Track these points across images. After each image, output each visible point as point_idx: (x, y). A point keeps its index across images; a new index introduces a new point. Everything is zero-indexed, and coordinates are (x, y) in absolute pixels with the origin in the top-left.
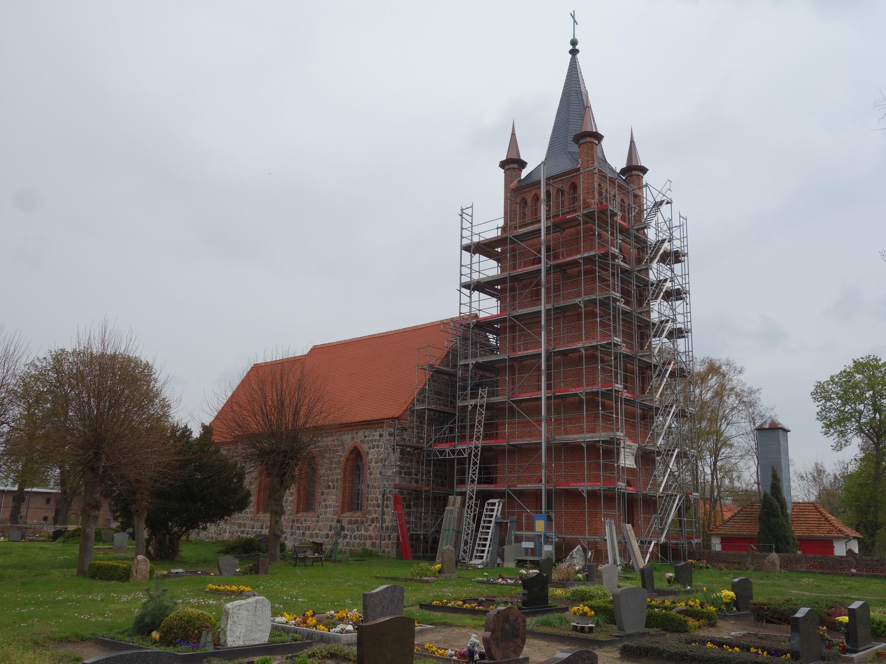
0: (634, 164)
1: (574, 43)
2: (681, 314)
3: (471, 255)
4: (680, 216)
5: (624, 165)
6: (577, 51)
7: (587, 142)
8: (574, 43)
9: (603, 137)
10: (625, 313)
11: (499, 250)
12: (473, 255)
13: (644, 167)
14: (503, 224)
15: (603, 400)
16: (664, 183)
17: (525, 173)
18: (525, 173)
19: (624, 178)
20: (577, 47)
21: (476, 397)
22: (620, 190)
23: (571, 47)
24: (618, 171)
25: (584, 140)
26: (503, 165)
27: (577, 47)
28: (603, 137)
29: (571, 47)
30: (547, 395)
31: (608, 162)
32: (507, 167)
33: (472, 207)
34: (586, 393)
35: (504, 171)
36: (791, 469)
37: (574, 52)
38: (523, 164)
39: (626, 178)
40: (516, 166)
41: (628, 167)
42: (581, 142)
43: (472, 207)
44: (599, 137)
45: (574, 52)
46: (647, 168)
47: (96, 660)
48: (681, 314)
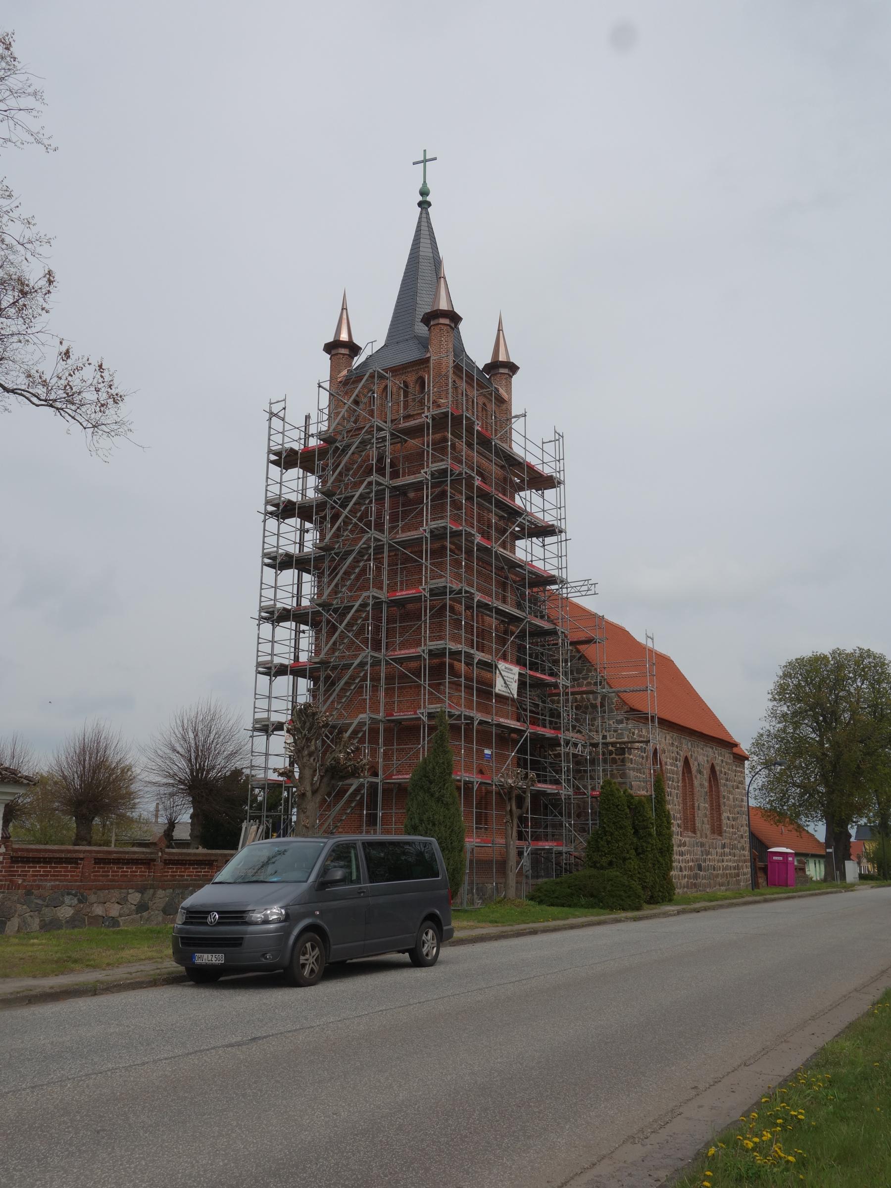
0: (502, 358)
1: (424, 193)
4: (555, 432)
5: (489, 360)
6: (429, 204)
8: (424, 193)
9: (519, 368)
10: (481, 548)
13: (513, 364)
14: (849, 650)
15: (452, 661)
17: (358, 361)
18: (358, 361)
19: (488, 377)
22: (479, 389)
24: (481, 367)
25: (436, 322)
26: (329, 348)
27: (428, 199)
28: (519, 368)
29: (420, 198)
32: (333, 352)
33: (284, 400)
34: (430, 651)
35: (329, 356)
36: (48, 991)
37: (424, 205)
38: (354, 349)
39: (490, 377)
43: (284, 400)
44: (455, 319)
45: (424, 205)
47: (195, 894)
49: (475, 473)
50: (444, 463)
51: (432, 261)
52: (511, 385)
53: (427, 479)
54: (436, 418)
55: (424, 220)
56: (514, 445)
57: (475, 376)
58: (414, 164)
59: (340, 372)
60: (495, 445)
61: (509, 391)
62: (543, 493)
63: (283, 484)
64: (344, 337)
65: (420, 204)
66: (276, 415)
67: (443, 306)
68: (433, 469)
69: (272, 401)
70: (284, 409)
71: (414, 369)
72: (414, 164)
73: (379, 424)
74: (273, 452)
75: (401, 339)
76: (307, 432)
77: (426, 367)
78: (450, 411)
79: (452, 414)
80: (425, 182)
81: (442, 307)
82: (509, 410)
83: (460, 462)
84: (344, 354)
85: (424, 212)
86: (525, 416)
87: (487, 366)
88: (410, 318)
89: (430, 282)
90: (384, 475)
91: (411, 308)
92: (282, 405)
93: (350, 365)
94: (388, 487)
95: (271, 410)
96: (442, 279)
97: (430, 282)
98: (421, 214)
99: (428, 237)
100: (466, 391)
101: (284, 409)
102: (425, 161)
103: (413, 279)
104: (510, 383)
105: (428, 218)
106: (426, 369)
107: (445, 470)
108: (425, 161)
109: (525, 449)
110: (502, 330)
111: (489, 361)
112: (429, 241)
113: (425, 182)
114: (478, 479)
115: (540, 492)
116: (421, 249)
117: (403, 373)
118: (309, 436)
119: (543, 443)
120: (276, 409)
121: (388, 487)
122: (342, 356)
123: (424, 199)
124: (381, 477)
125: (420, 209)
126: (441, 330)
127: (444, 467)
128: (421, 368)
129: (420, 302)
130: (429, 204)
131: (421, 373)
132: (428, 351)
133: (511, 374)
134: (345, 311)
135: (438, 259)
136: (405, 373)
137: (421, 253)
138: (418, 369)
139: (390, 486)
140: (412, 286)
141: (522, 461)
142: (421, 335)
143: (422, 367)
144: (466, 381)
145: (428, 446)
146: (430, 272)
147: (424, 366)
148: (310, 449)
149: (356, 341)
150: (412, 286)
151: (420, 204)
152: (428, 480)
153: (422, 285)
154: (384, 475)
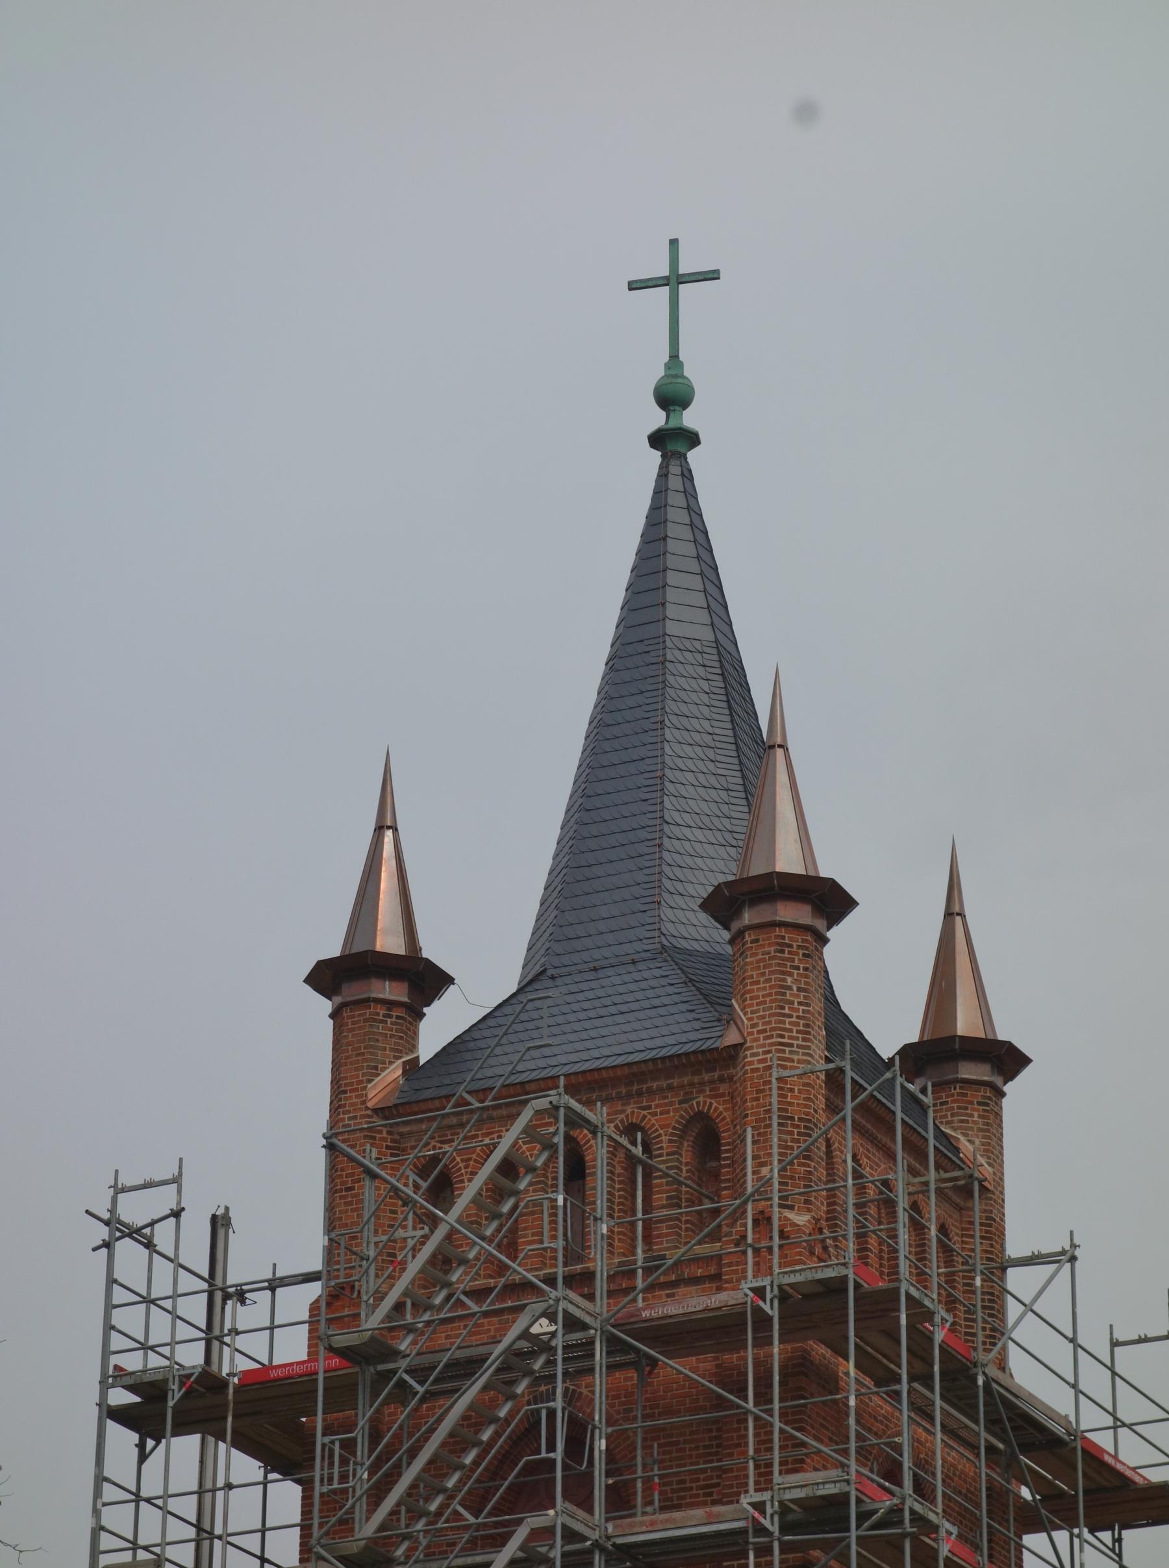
0: (965, 1024)
2: (1124, 1425)
3: (141, 1446)
6: (693, 439)
7: (782, 924)
9: (858, 904)
11: (304, 1419)
12: (150, 1443)
13: (832, 885)
16: (637, 607)
20: (690, 419)
21: (783, 1411)
23: (657, 419)
27: (690, 419)
29: (657, 419)
30: (847, 1534)
31: (843, 1008)
32: (352, 991)
33: (177, 1180)
40: (391, 990)
41: (341, 956)
42: (748, 917)
43: (177, 1180)
46: (308, 989)
48: (1124, 1425)
49: (939, 1510)
50: (833, 1473)
51: (712, 659)
52: (1000, 1126)
53: (761, 1530)
54: (791, 1296)
55: (676, 499)
56: (1017, 1361)
57: (899, 1115)
58: (633, 286)
59: (375, 1071)
60: (987, 1384)
61: (994, 1148)
62: (1119, 1540)
63: (133, 1497)
64: (389, 941)
65: (657, 440)
66: (133, 1233)
67: (788, 861)
68: (788, 1496)
69: (125, 1180)
70: (176, 1214)
71: (675, 1082)
72: (633, 286)
73: (572, 1309)
74: (129, 1381)
75: (606, 952)
76: (219, 1282)
77: (721, 1080)
78: (851, 1277)
79: (857, 1286)
80: (674, 356)
81: (962, 1028)
82: (994, 1231)
83: (892, 1473)
84: (390, 1004)
85: (675, 469)
86: (1073, 1259)
87: (907, 1051)
88: (640, 877)
89: (708, 739)
90: (586, 1504)
91: (642, 834)
92: (165, 1198)
93: (411, 1040)
94: (603, 1550)
95: (113, 1211)
96: (780, 753)
97: (708, 739)
98: (663, 474)
99: (694, 566)
100: (855, 1158)
101: (176, 1214)
102: (674, 280)
103: (646, 725)
104: (998, 1116)
105: (690, 493)
106: (724, 1088)
107: (841, 1501)
108: (674, 280)
109: (1074, 1386)
110: (961, 914)
111: (914, 1038)
112: (696, 582)
113: (674, 356)
114: (949, 1533)
115: (1106, 1536)
116: (671, 611)
117: (629, 1095)
118: (226, 1297)
119: (1115, 1344)
120: (134, 1210)
121: (603, 1550)
122: (382, 1011)
123: (673, 424)
124: (581, 1514)
125: (656, 456)
126: (782, 946)
127: (831, 1490)
128: (702, 1083)
129: (677, 817)
130: (693, 439)
131: (702, 1101)
132: (731, 1019)
133: (820, 924)
134: (389, 834)
135: (731, 648)
136: (640, 1094)
137: (671, 628)
138: (692, 1084)
139: (609, 1545)
140: (643, 752)
141: (1060, 1431)
142: (684, 944)
143: (706, 1077)
144: (856, 1127)
145: (763, 1397)
146: (705, 698)
147: (716, 1075)
148: (273, 1374)
149: (430, 950)
150: (643, 752)
151: (657, 440)
152: (767, 1533)
153: (677, 747)
154: (586, 1504)
